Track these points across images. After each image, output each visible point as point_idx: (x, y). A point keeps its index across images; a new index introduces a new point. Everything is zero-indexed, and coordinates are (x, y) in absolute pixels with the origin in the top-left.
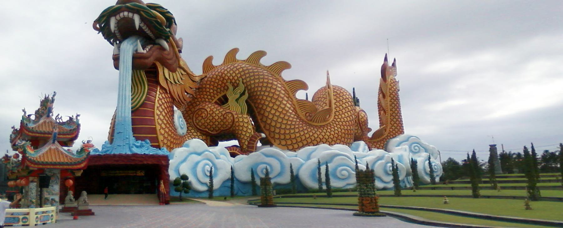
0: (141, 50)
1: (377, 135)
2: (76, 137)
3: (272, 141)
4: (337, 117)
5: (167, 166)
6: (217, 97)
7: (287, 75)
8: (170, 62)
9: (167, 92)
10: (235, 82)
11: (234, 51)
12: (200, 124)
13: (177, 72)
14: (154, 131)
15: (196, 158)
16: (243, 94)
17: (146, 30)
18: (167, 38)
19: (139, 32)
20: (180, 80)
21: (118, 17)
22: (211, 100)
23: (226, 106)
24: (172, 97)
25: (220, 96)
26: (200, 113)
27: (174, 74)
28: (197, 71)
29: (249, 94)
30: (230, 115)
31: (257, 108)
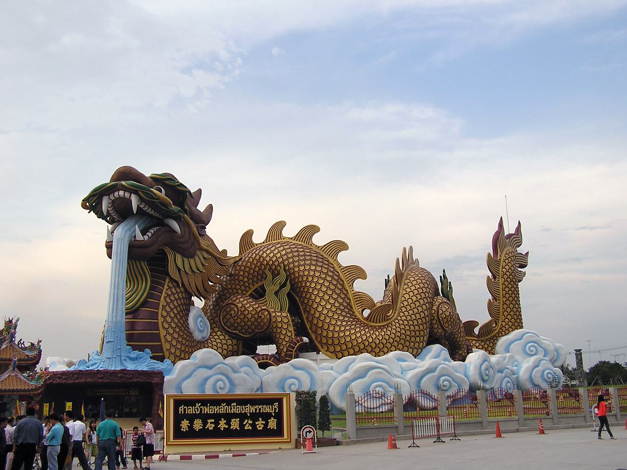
0: (140, 237)
2: (38, 362)
4: (402, 314)
5: (161, 384)
6: (253, 288)
8: (184, 246)
9: (179, 285)
10: (276, 268)
12: (228, 324)
13: (196, 257)
14: (157, 338)
15: (205, 372)
16: (283, 286)
17: (145, 209)
20: (200, 267)
21: (112, 197)
22: (244, 292)
23: (262, 300)
25: (257, 286)
26: (229, 309)
27: (192, 261)
28: (233, 252)
30: (266, 313)
31: (303, 303)
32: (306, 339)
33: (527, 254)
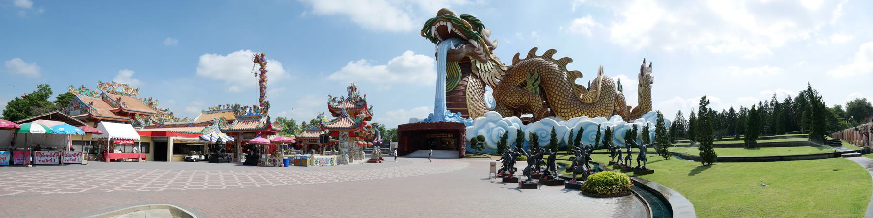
1: (635, 110)
5: (464, 131)
7: (570, 67)
11: (517, 55)
14: (465, 105)
18: (476, 39)
19: (457, 39)
24: (482, 81)
28: (507, 62)
29: (542, 82)
32: (549, 110)
33: (810, 88)
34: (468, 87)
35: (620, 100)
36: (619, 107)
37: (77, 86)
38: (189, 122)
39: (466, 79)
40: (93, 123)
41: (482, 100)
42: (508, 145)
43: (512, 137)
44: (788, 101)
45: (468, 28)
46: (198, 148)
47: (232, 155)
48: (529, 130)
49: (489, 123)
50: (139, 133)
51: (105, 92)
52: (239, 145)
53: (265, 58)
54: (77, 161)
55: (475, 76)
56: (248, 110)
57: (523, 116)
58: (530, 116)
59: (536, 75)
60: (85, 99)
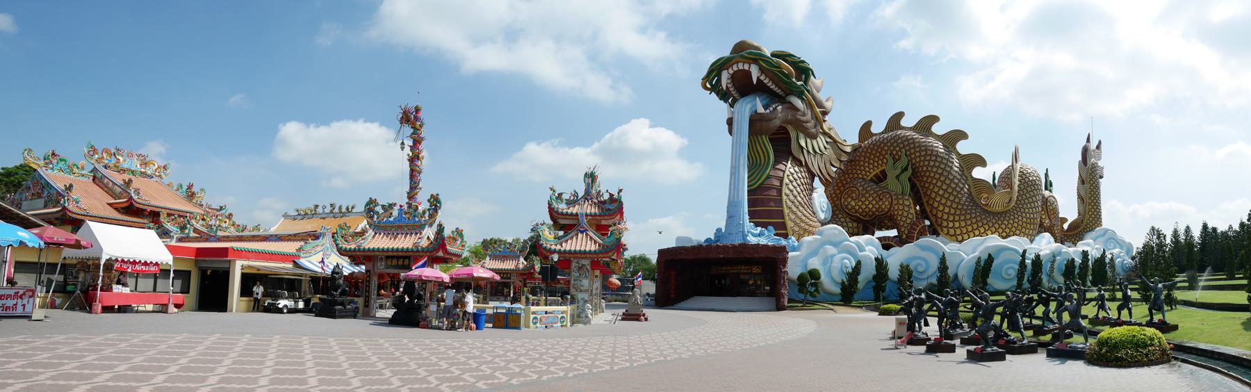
1: (1074, 226)
3: (939, 229)
5: (784, 261)
7: (963, 147)
11: (868, 125)
16: (906, 169)
18: (800, 95)
19: (765, 91)
24: (809, 171)
25: (877, 171)
28: (850, 138)
29: (913, 170)
32: (927, 223)
34: (786, 180)
35: (1049, 207)
36: (1048, 220)
37: (40, 152)
38: (261, 232)
39: (781, 166)
40: (70, 228)
41: (810, 205)
42: (860, 286)
43: (868, 271)
44: (1242, 225)
45: (788, 76)
46: (290, 285)
47: (360, 301)
48: (896, 258)
49: (824, 246)
50: (172, 249)
51: (100, 167)
52: (375, 282)
53: (421, 115)
54: (20, 310)
55: (798, 162)
56: (395, 212)
57: (879, 234)
58: (893, 233)
59: (904, 161)
60: (56, 178)
